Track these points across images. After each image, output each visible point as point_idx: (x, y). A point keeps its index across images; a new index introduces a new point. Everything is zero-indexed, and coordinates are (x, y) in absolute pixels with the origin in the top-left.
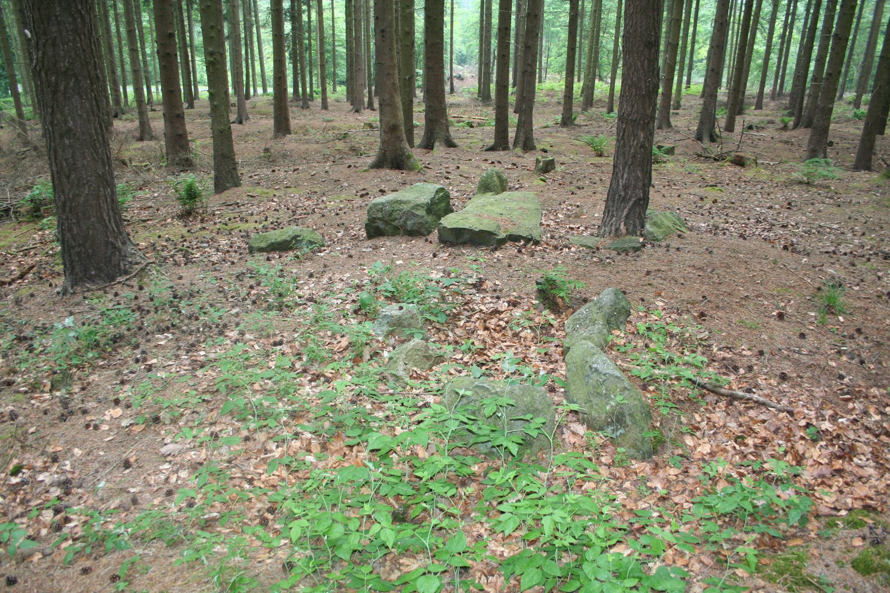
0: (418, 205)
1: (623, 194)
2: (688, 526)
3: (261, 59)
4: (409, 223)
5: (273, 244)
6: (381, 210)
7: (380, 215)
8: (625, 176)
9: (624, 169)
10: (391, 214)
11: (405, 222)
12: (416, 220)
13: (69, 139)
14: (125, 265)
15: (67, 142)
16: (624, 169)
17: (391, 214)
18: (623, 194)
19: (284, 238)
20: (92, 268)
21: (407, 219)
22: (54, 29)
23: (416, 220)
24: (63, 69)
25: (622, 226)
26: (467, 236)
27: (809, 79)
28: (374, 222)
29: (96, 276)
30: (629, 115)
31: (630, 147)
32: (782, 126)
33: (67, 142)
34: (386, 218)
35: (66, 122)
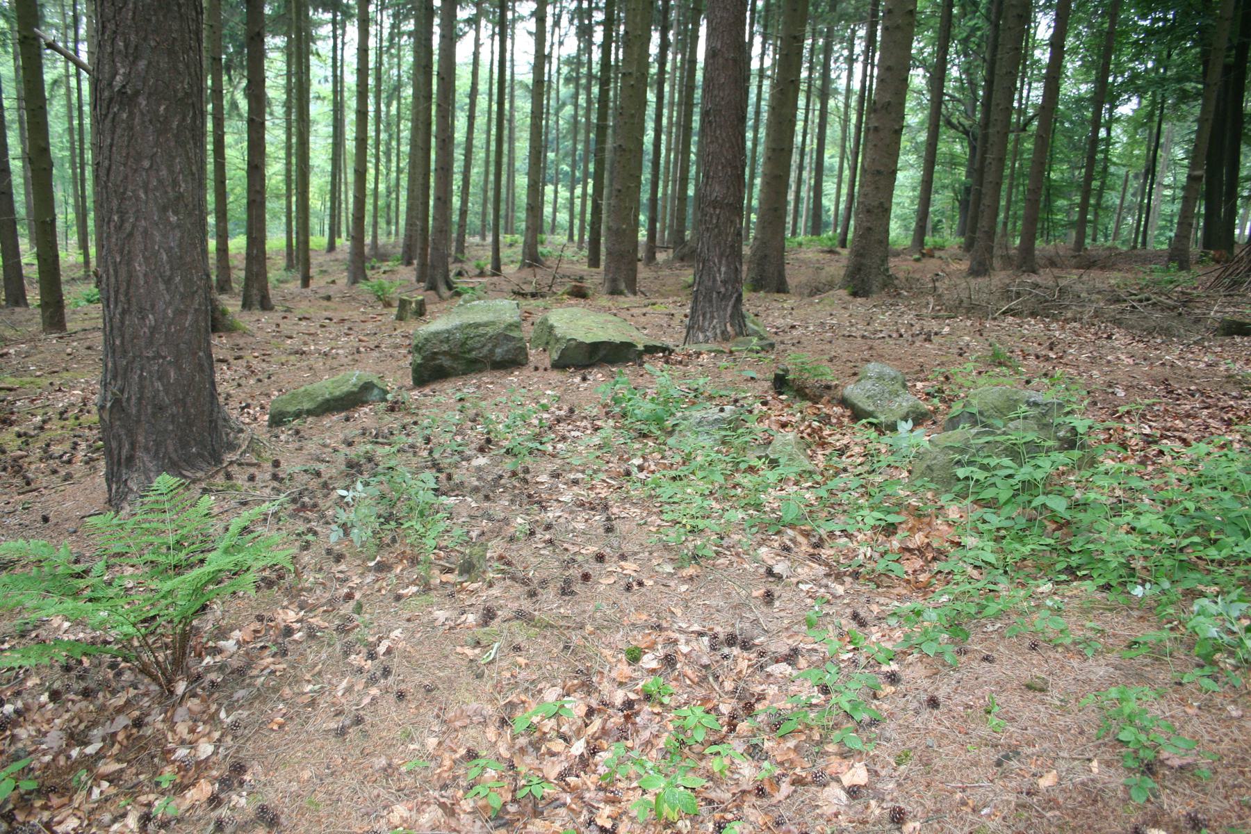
0: (511, 325)
1: (723, 290)
2: (938, 611)
3: (490, 95)
4: (498, 351)
5: (328, 401)
6: (447, 340)
7: (445, 347)
8: (723, 269)
9: (720, 262)
10: (465, 343)
11: (492, 351)
12: (511, 345)
13: (176, 213)
14: (228, 434)
15: (173, 219)
16: (720, 262)
17: (465, 343)
18: (723, 290)
19: (345, 389)
20: (193, 443)
21: (495, 346)
22: (175, 26)
23: (511, 345)
24: (180, 95)
25: (729, 328)
26: (602, 353)
27: (431, 219)
28: (434, 359)
29: (199, 455)
30: (724, 198)
31: (727, 235)
32: (478, 271)
33: (173, 219)
34: (456, 351)
35: (175, 183)
